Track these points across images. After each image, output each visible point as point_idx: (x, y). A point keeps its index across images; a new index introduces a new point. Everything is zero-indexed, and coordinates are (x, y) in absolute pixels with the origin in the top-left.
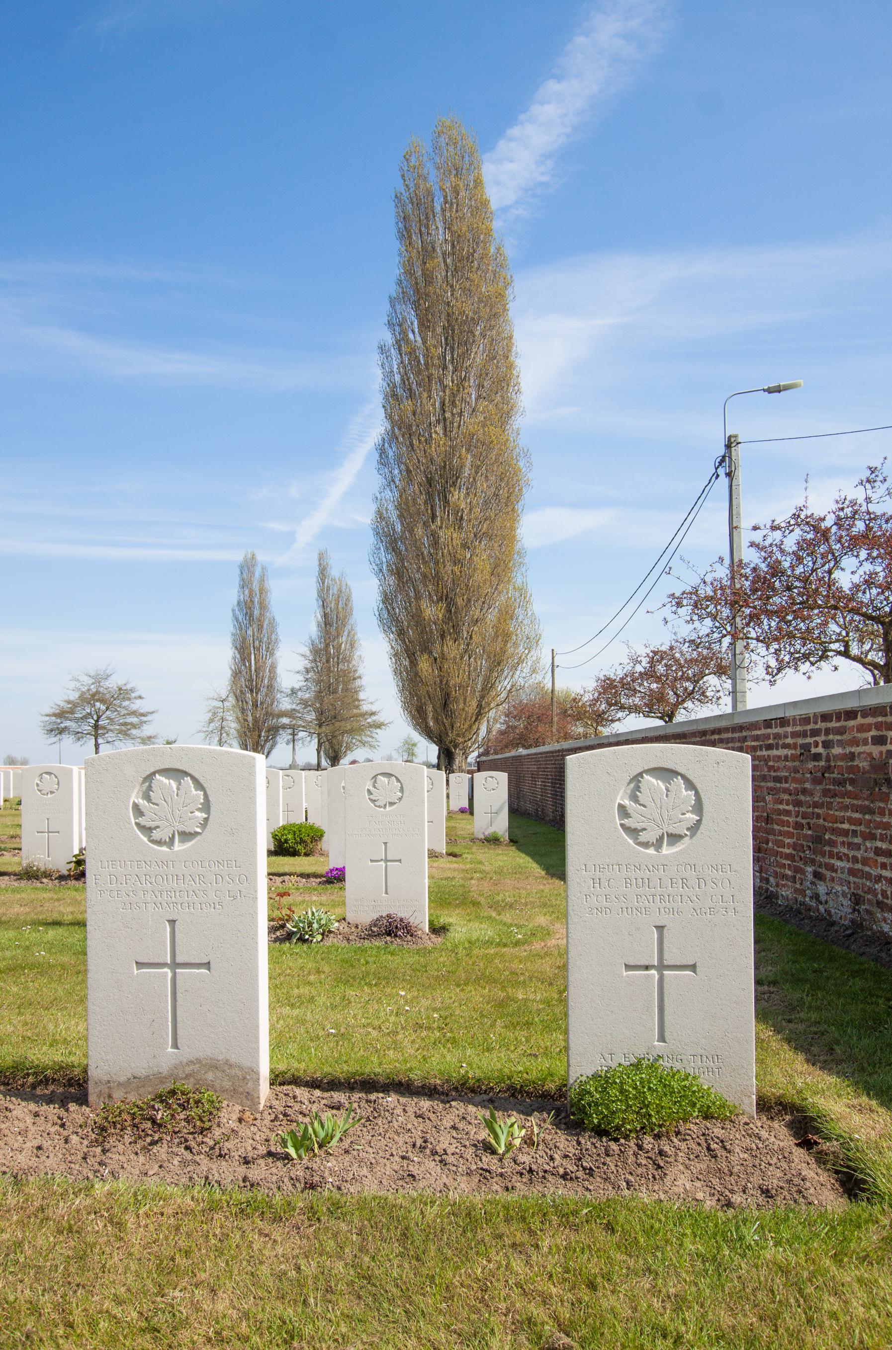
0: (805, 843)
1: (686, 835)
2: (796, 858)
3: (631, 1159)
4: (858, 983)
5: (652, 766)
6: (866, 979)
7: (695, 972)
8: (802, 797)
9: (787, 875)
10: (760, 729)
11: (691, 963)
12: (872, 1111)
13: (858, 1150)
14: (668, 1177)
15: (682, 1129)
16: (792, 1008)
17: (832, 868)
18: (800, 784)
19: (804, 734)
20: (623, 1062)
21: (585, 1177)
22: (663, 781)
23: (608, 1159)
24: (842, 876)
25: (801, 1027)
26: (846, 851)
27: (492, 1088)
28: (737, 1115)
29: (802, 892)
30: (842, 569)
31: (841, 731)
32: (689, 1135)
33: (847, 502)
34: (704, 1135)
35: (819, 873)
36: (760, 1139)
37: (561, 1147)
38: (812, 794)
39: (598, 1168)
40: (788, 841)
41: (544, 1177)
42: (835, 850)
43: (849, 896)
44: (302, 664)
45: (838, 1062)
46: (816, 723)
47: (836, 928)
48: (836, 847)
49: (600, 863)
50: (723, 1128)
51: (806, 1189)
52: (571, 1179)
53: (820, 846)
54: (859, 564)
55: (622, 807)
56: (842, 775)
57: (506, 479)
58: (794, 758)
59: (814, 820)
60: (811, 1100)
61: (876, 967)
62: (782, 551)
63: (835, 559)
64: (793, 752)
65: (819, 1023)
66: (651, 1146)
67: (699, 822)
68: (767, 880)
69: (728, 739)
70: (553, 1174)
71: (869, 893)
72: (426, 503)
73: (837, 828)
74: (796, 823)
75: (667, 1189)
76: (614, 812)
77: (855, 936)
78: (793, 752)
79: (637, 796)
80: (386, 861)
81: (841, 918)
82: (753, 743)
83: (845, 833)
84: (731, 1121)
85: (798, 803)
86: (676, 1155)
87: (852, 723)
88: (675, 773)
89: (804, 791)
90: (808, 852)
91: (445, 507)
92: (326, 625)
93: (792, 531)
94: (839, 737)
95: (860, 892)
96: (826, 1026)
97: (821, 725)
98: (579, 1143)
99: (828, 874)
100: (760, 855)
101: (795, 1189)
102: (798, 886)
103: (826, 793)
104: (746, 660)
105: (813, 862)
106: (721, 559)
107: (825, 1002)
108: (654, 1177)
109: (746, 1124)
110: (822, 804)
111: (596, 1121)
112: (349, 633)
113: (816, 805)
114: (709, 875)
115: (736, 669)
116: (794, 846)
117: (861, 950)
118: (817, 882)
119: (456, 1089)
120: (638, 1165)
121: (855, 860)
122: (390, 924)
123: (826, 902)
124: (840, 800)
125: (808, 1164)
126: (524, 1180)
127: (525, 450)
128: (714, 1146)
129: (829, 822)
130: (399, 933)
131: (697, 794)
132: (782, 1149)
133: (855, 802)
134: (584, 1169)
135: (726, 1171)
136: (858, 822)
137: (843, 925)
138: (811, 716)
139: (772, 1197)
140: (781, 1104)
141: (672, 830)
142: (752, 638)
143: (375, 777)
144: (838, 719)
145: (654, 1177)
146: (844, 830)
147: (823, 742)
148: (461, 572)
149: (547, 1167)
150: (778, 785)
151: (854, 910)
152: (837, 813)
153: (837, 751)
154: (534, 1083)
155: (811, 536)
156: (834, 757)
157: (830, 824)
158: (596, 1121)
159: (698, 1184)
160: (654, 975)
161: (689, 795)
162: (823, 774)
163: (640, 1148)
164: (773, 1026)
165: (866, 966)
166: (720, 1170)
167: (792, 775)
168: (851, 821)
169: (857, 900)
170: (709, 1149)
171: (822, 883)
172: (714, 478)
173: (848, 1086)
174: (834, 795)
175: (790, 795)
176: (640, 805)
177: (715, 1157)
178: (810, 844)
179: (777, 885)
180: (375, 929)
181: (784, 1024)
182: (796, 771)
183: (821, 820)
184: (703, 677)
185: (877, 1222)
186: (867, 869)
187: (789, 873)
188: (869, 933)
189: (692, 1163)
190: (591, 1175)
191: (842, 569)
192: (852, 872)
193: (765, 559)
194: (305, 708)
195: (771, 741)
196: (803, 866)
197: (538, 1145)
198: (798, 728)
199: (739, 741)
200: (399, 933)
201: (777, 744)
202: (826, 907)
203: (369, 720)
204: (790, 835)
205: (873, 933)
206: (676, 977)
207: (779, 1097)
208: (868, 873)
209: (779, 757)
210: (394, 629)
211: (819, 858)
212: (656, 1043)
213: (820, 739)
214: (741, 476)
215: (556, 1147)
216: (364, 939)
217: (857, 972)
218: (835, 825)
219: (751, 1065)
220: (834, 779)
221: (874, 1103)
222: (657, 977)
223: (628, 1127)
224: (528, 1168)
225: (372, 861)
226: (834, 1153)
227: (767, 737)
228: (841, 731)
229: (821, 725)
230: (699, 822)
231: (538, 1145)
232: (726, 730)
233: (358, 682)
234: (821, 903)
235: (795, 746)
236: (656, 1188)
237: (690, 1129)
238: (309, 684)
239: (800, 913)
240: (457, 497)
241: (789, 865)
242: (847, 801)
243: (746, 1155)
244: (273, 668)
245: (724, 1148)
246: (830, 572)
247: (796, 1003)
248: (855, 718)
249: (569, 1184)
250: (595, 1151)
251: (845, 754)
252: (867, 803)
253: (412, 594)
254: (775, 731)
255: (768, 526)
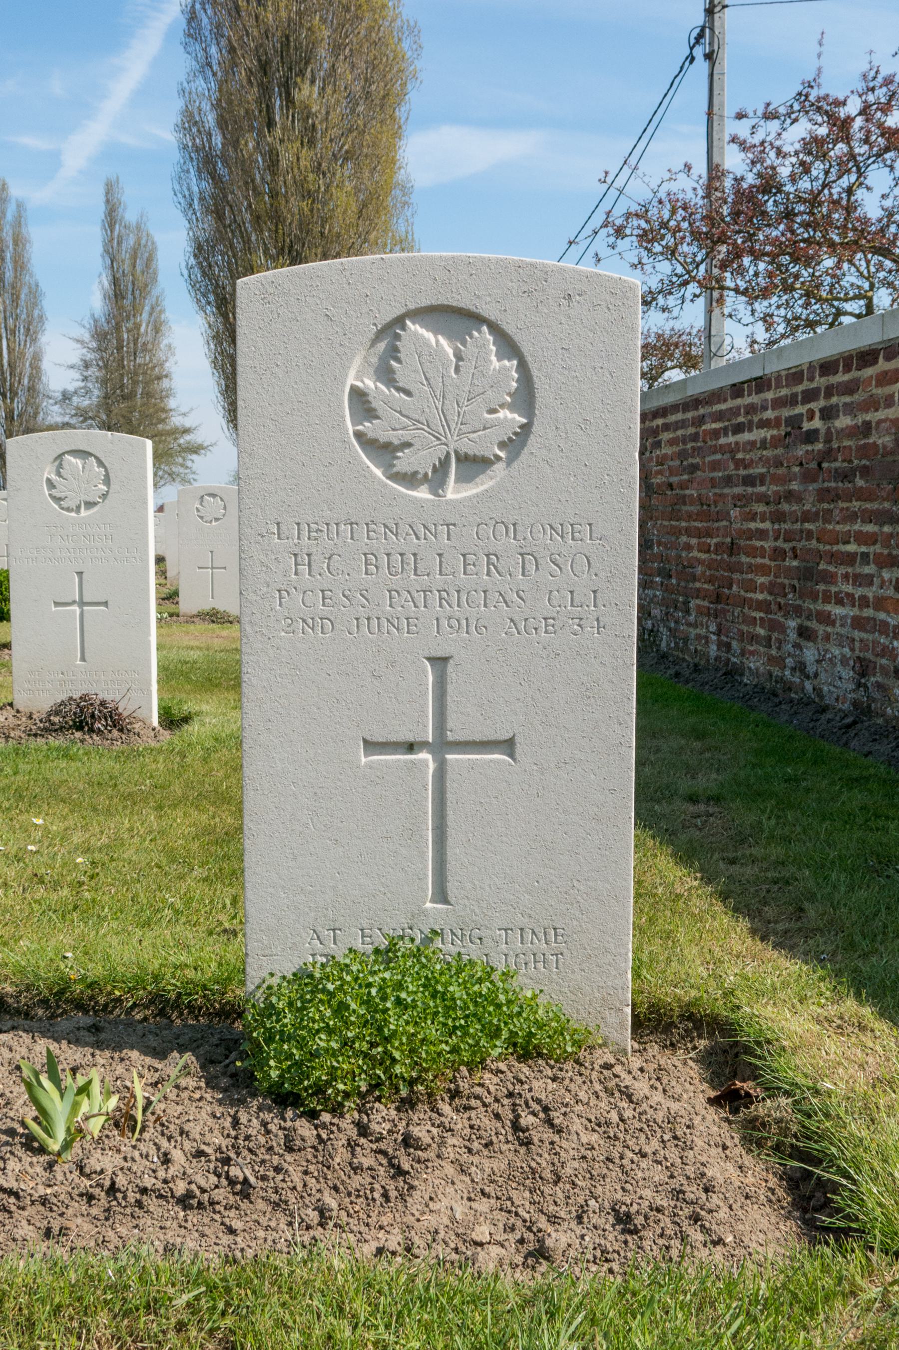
0: (786, 582)
1: (498, 458)
2: (773, 606)
3: (341, 1156)
4: (857, 798)
5: (425, 302)
6: (871, 792)
7: (512, 755)
8: (785, 507)
9: (758, 636)
10: (725, 400)
11: (505, 736)
12: (862, 1028)
13: (827, 1115)
14: (416, 1194)
15: (464, 1085)
16: (741, 840)
17: (826, 619)
18: (782, 485)
19: (792, 401)
20: (359, 946)
21: (232, 1199)
22: (450, 337)
23: (289, 1157)
24: (843, 631)
25: (750, 871)
26: (848, 588)
27: (119, 1000)
28: (591, 1048)
29: (779, 661)
30: (868, 189)
31: (850, 388)
32: (477, 1097)
33: (880, 79)
34: (510, 1095)
35: (807, 628)
36: (630, 1098)
37: (195, 1133)
38: (801, 499)
39: (264, 1178)
40: (761, 580)
41: (139, 1204)
42: (834, 589)
43: (851, 663)
44: (75, 354)
45: (808, 933)
46: (811, 379)
47: (829, 715)
48: (835, 583)
49: (310, 519)
50: (554, 1079)
51: (710, 1211)
52: (200, 1205)
53: (809, 584)
54: (893, 183)
55: (358, 395)
56: (850, 462)
57: (381, 67)
58: (776, 442)
59: (804, 542)
60: (748, 1010)
61: (889, 773)
62: (779, 152)
63: (859, 169)
64: (775, 432)
65: (783, 863)
66: (387, 1126)
67: (526, 428)
68: (728, 646)
69: (677, 422)
70: (160, 1196)
71: (883, 656)
72: (259, 102)
73: (838, 552)
74: (775, 550)
75: (410, 1220)
76: (340, 406)
77: (859, 726)
78: (775, 432)
79: (391, 371)
80: (82, 603)
81: (837, 699)
82: (714, 426)
83: (850, 559)
84: (577, 1062)
85: (779, 517)
86: (442, 1144)
87: (869, 372)
88: (476, 319)
89: (790, 496)
90: (790, 596)
91: (288, 109)
92: (116, 296)
93: (795, 121)
94: (847, 399)
95: (869, 655)
96: (794, 869)
97: (820, 382)
98: (236, 1123)
99: (821, 629)
100: (719, 607)
101: (687, 1211)
102: (774, 652)
103: (824, 495)
104: (726, 343)
105: (798, 611)
106: (688, 167)
107: (799, 829)
108: (386, 1196)
109: (608, 1066)
110: (817, 514)
111: (274, 1074)
112: (153, 308)
113: (806, 517)
114: (546, 547)
115: (711, 359)
116: (771, 589)
117: (866, 749)
118: (803, 643)
119: (44, 1002)
120: (355, 1169)
121: (864, 602)
122: (82, 711)
123: (816, 675)
124: (845, 505)
125: (725, 1148)
126: (94, 1211)
127: (412, 23)
128: (527, 1120)
129: (826, 543)
130: (97, 725)
131: (523, 367)
132: (672, 1119)
133: (868, 506)
134: (232, 1182)
135: (547, 1175)
136: (870, 539)
137: (840, 710)
138: (805, 368)
139: (635, 1231)
140: (691, 1017)
141: (467, 447)
142: (729, 289)
143: (60, 457)
144: (848, 369)
145: (386, 1196)
146: (849, 554)
147: (821, 410)
148: (311, 210)
149: (148, 1182)
150: (750, 490)
151: (859, 685)
152: (838, 527)
153: (843, 422)
154: (205, 988)
155: (823, 131)
156: (838, 432)
157: (828, 547)
158: (274, 1074)
159: (483, 1205)
160: (425, 762)
161: (504, 370)
162: (819, 465)
163: (363, 1130)
164: (701, 870)
165: (872, 771)
166: (534, 1172)
167: (772, 470)
168: (862, 539)
169: (863, 668)
170: (516, 1126)
171: (811, 644)
172: (687, 63)
173: (822, 979)
174: (837, 497)
175: (767, 504)
176: (398, 389)
177: (527, 1143)
178: (795, 582)
179: (743, 654)
180: (56, 719)
181: (722, 865)
182: (778, 464)
183: (814, 542)
184: (663, 372)
185: (853, 1294)
186: (882, 616)
187: (762, 632)
188: (880, 721)
189: (476, 1159)
190: (247, 1196)
191: (868, 189)
192: (858, 623)
193: (753, 163)
194: (83, 422)
195: (741, 419)
196: (782, 620)
197: (143, 1129)
198: (784, 392)
199: (693, 424)
200: (97, 725)
201: (751, 422)
202: (816, 682)
203: (181, 441)
204: (763, 570)
205: (887, 721)
206: (472, 765)
207: (689, 1004)
208: (885, 624)
209: (753, 443)
210: (212, 298)
211: (808, 605)
212: (429, 905)
213: (815, 406)
214: (727, 59)
215: (182, 1132)
216: (35, 735)
217: (857, 780)
218: (835, 548)
219: (625, 946)
220: (836, 470)
221: (867, 1011)
222: (432, 766)
223: (341, 1087)
224: (107, 1183)
225: (57, 604)
226: (779, 1121)
227: (735, 412)
228: (850, 388)
229: (820, 382)
230: (526, 428)
231: (143, 1129)
232: (674, 408)
233: (165, 383)
234: (808, 677)
235: (777, 423)
236: (385, 1220)
237: (481, 1085)
238: (90, 385)
239: (775, 695)
240: (306, 92)
241: (761, 619)
242: (856, 505)
243: (595, 1136)
244: (37, 358)
245: (549, 1122)
246: (850, 191)
247: (748, 832)
248: (875, 361)
249: (193, 1217)
250: (262, 1140)
251: (856, 426)
252: (887, 505)
253: (239, 247)
254: (748, 400)
255: (760, 113)
